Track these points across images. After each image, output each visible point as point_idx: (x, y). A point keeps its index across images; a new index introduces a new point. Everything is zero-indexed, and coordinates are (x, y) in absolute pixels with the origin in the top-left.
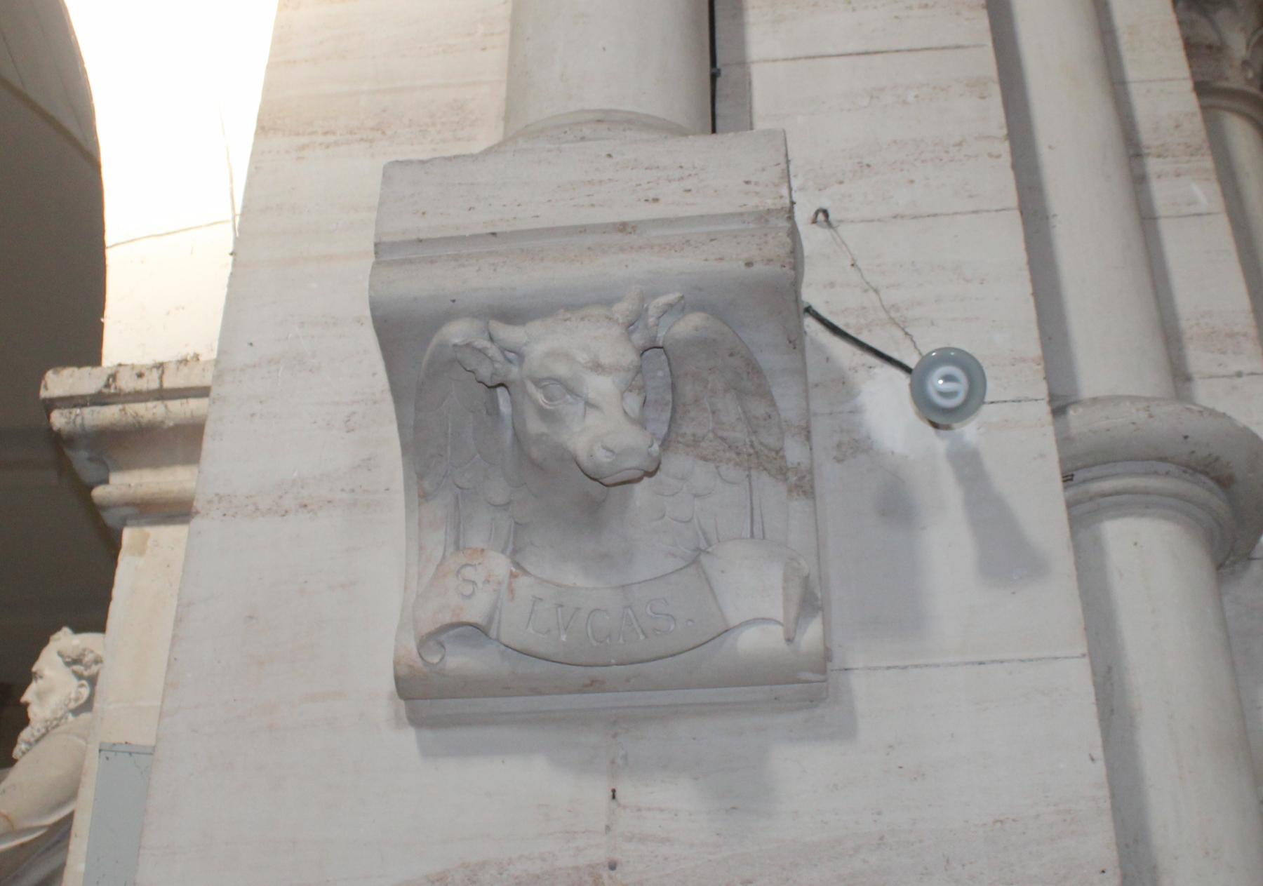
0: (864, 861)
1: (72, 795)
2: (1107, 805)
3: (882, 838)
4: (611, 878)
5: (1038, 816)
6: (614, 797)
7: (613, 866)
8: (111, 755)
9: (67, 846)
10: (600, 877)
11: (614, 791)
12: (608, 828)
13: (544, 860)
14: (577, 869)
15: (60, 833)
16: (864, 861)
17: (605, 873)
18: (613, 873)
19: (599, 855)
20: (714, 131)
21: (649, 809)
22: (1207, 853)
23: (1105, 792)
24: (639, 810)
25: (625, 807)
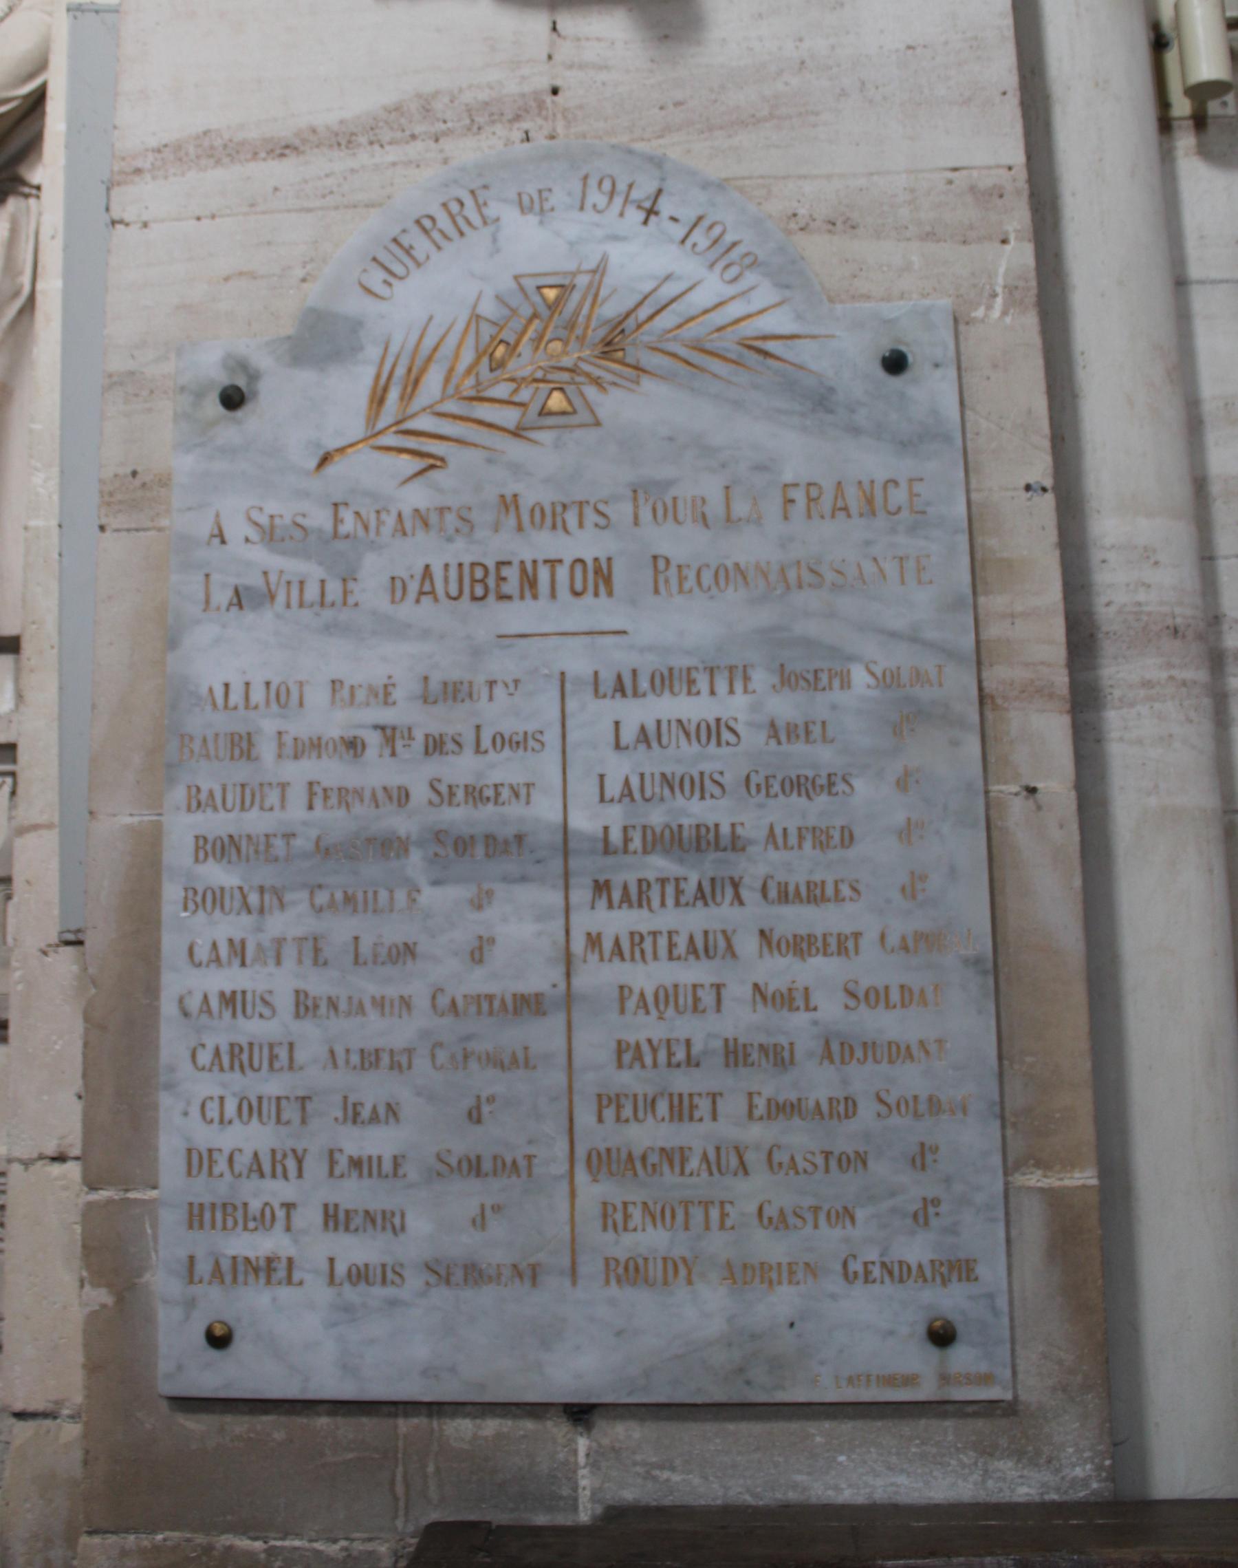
0: (786, 84)
1: (42, 65)
2: (1010, 33)
3: (803, 63)
4: (553, 102)
5: (946, 43)
6: (554, 29)
7: (555, 91)
8: (78, 14)
9: (43, 114)
10: (544, 102)
11: (554, 23)
12: (550, 57)
13: (491, 88)
14: (523, 95)
15: (38, 100)
16: (786, 84)
17: (549, 99)
18: (555, 98)
19: (544, 83)
20: (563, 674)
21: (587, 39)
22: (1097, 85)
23: (1009, 21)
24: (578, 39)
25: (564, 38)
